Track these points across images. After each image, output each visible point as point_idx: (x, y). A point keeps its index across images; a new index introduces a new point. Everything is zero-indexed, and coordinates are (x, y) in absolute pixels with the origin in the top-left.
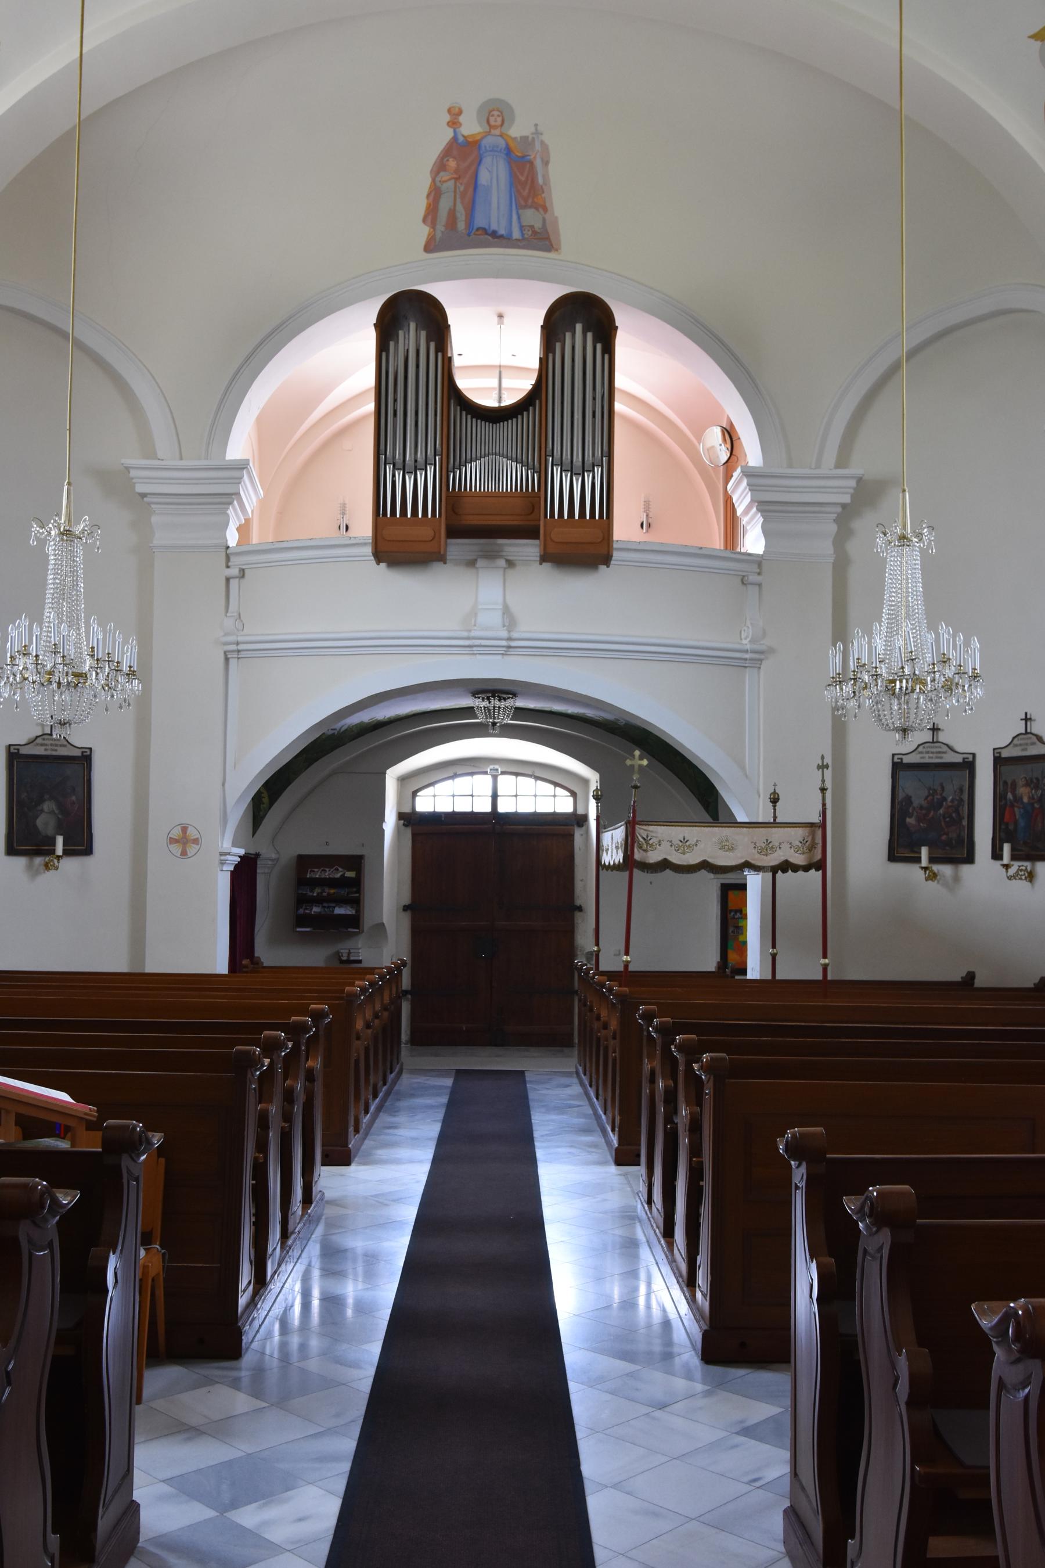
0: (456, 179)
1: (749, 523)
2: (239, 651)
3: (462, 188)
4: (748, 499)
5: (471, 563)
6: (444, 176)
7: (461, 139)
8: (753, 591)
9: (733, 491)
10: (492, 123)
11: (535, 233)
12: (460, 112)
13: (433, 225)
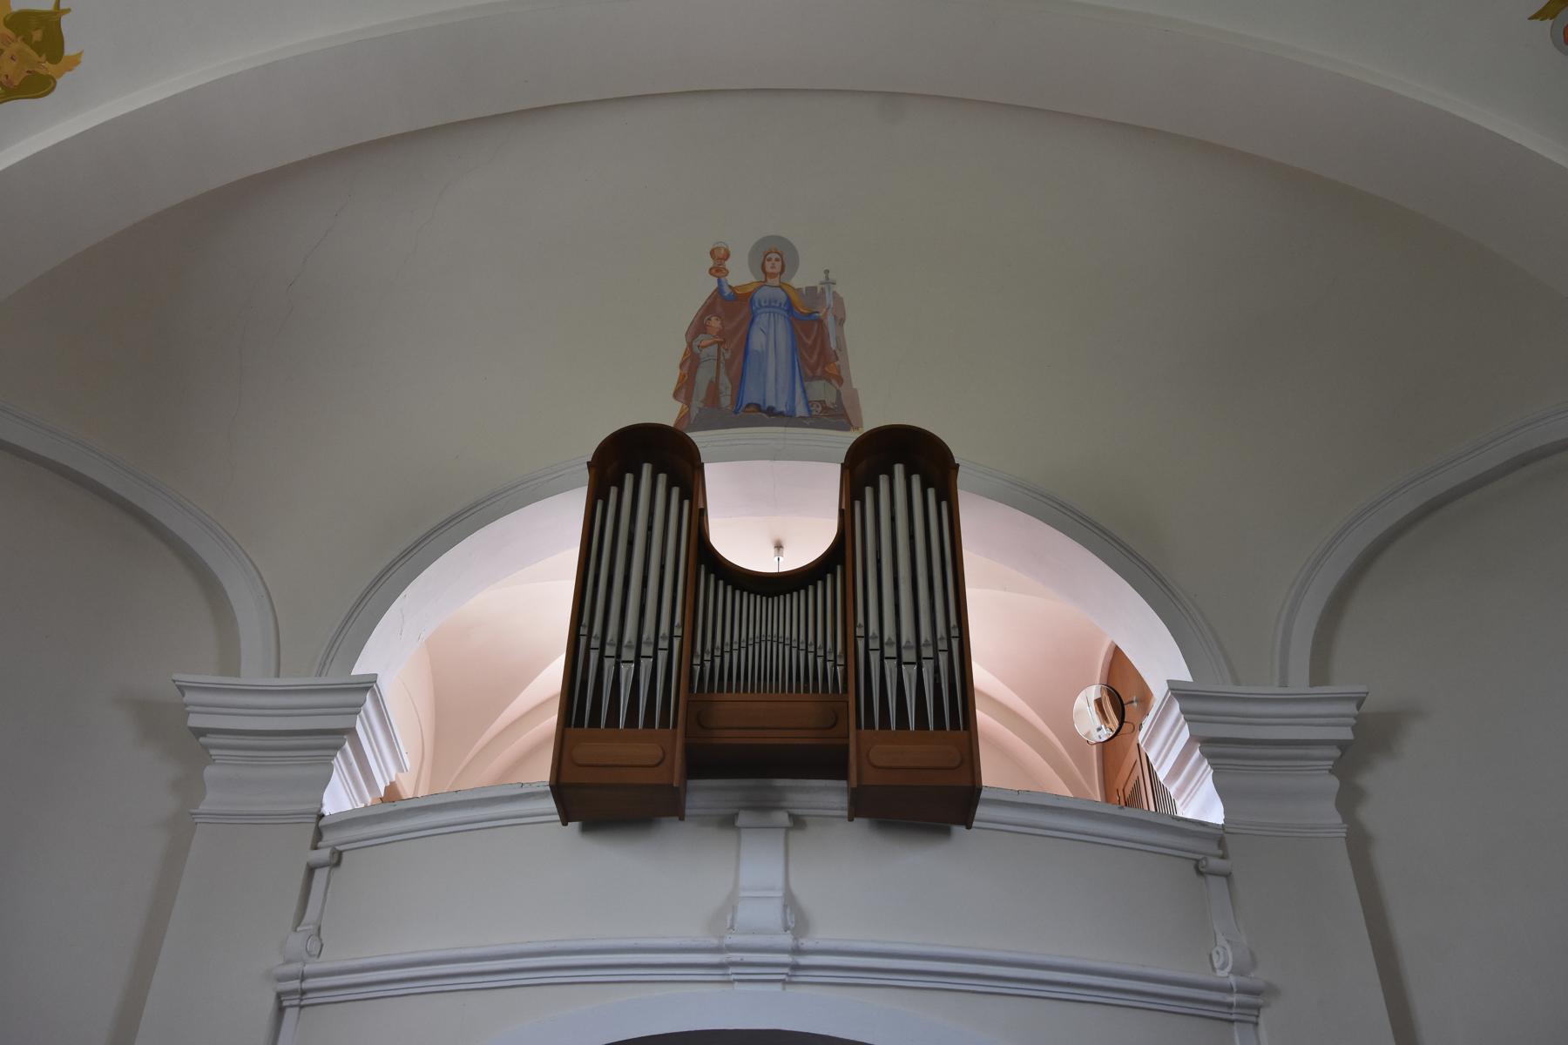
0: (720, 344)
1: (1181, 790)
2: (303, 992)
3: (728, 356)
4: (1185, 734)
5: (728, 822)
6: (703, 339)
7: (727, 291)
8: (1217, 884)
9: (1149, 743)
10: (768, 269)
11: (825, 408)
12: (727, 256)
13: (688, 401)
